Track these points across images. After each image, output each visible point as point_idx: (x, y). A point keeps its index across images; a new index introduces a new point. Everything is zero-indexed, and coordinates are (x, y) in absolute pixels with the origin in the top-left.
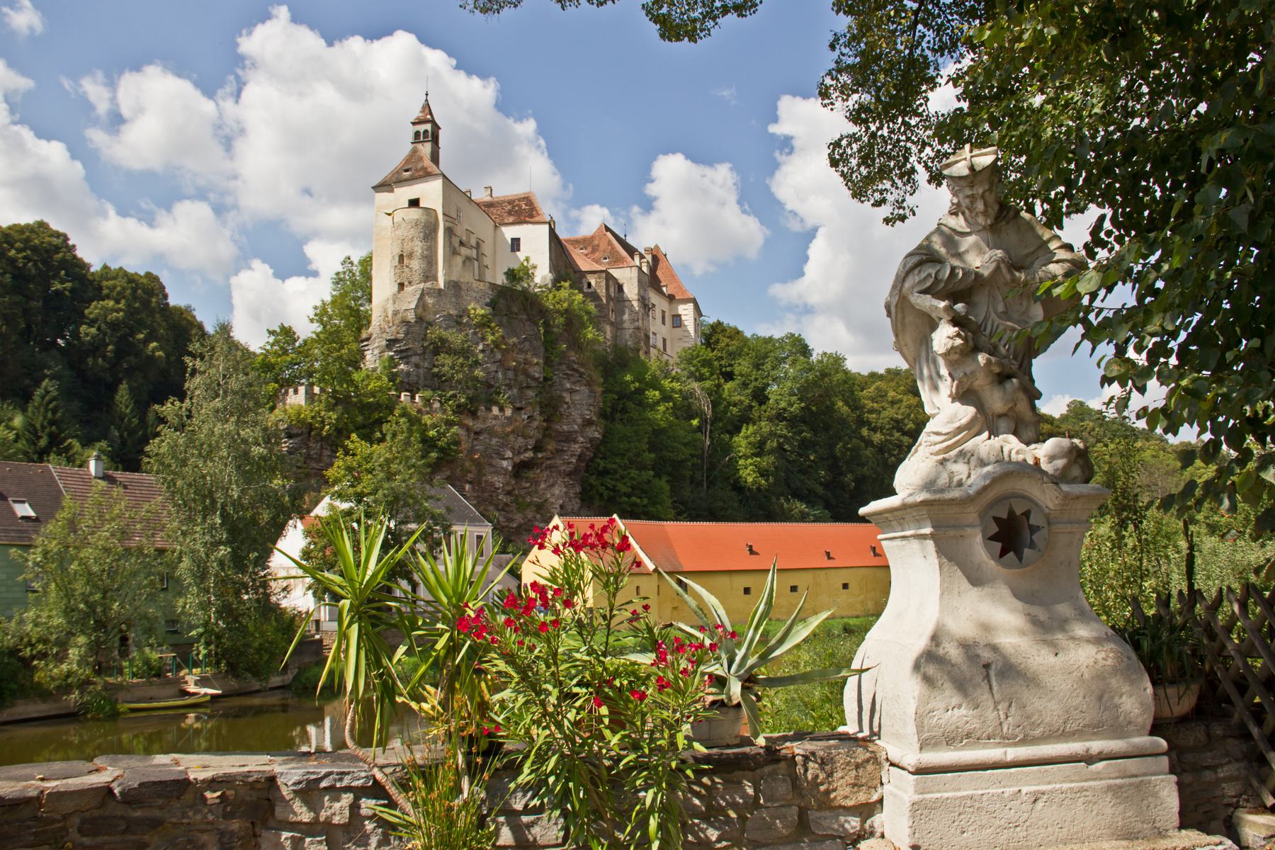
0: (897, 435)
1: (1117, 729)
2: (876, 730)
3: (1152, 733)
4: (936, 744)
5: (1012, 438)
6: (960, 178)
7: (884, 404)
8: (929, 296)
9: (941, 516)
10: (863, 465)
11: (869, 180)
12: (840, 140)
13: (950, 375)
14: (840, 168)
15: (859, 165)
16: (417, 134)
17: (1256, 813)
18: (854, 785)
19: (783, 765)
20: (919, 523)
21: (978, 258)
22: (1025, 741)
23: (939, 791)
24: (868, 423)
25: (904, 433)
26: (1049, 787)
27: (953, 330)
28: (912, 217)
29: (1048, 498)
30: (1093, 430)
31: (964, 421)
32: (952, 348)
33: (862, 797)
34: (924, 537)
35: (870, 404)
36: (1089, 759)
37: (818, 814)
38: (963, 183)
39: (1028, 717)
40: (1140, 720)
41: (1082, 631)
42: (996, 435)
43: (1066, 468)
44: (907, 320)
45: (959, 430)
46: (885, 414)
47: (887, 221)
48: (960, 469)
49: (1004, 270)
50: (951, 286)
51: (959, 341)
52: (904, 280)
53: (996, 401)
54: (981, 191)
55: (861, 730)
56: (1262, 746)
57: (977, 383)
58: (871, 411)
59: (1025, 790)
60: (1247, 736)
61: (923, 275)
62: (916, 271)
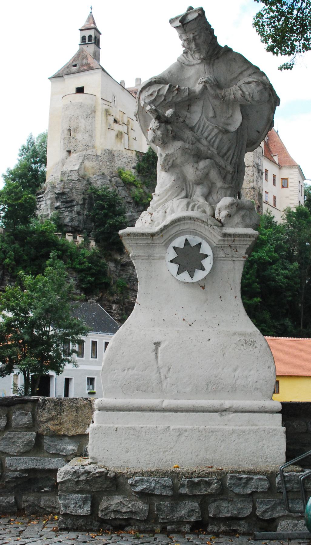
16: (83, 39)
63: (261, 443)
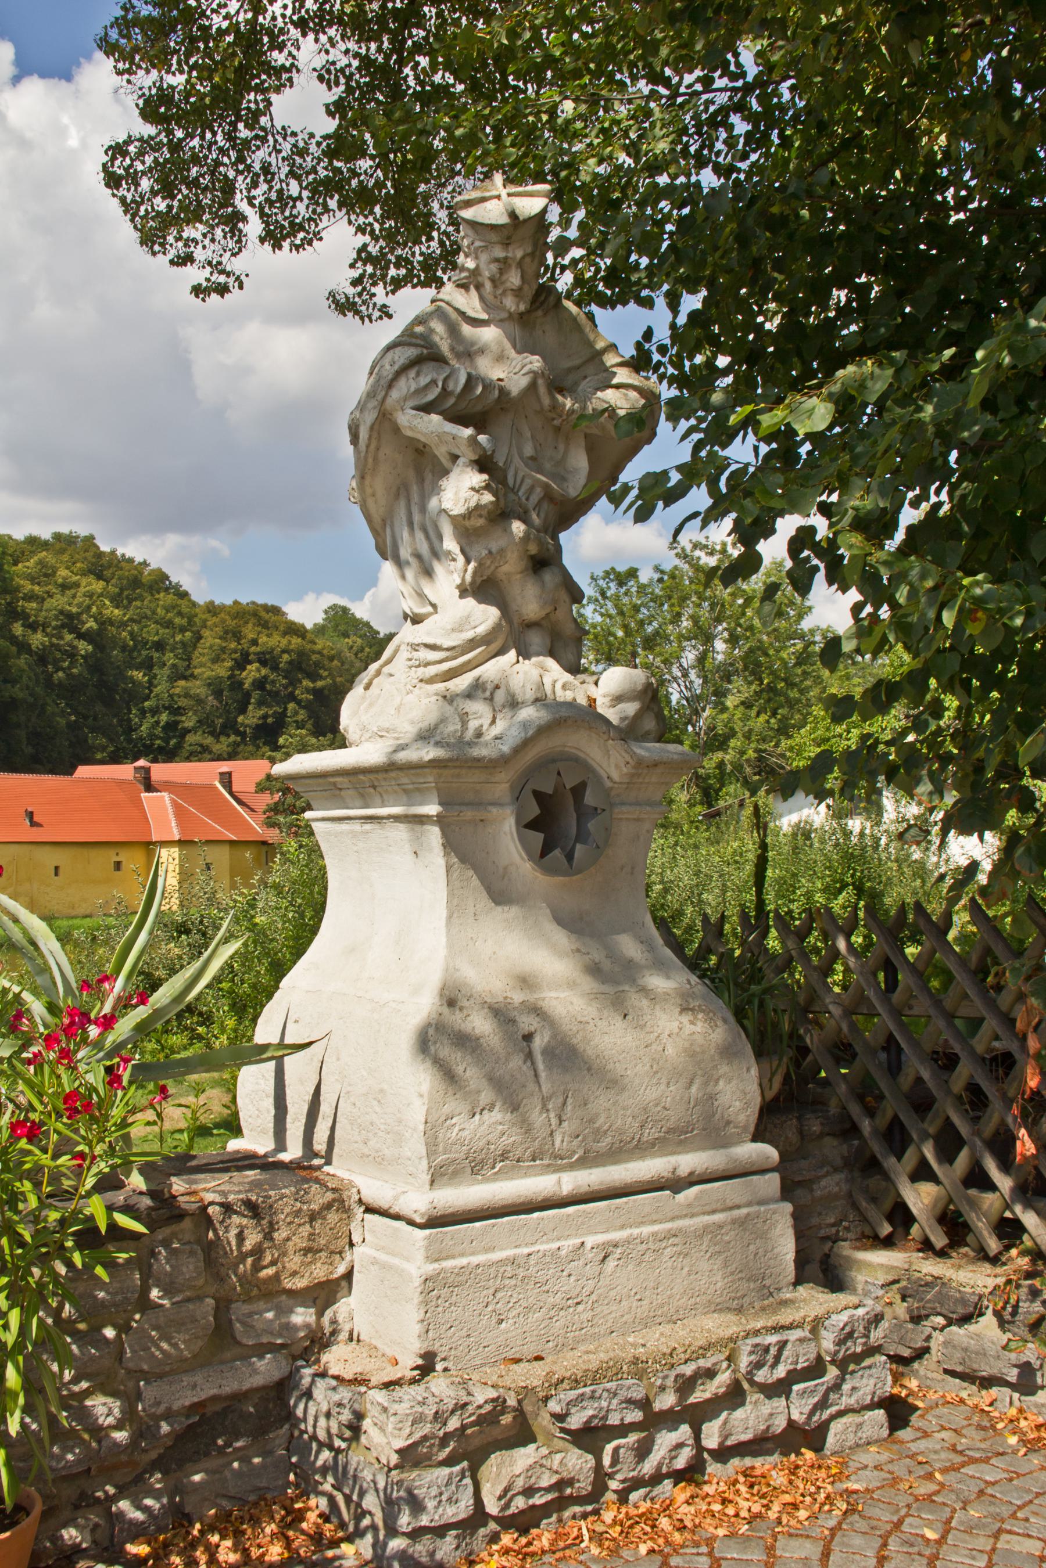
0: (69, 637)
1: (712, 1131)
2: (320, 1143)
3: (755, 1139)
4: (455, 1174)
5: (550, 663)
6: (493, 227)
7: (50, 588)
8: (435, 418)
9: (447, 783)
10: (14, 682)
11: (168, 221)
12: (129, 141)
13: (462, 551)
14: (122, 192)
15: (154, 193)
17: (865, 1249)
18: (307, 1251)
19: (187, 1224)
20: (412, 794)
21: (506, 365)
22: (586, 1161)
23: (462, 1255)
24: (23, 616)
25: (81, 636)
26: (623, 1234)
27: (478, 479)
28: (236, 291)
29: (610, 763)
30: (362, 650)
31: (481, 630)
32: (478, 507)
33: (319, 1272)
34: (420, 820)
35: (28, 586)
36: (675, 1184)
37: (246, 1308)
38: (494, 237)
39: (592, 1121)
40: (742, 1118)
41: (658, 983)
42: (527, 656)
43: (638, 716)
44: (381, 454)
45: (472, 644)
46: (50, 603)
47: (197, 290)
48: (479, 712)
49: (542, 389)
50: (463, 405)
51: (488, 498)
52: (390, 385)
53: (530, 602)
54: (519, 254)
55: (281, 1145)
56: (876, 1147)
57: (505, 568)
58: (30, 597)
59: (590, 1241)
60: (853, 1130)
61: (424, 381)
62: (412, 373)
63: (752, 1247)
